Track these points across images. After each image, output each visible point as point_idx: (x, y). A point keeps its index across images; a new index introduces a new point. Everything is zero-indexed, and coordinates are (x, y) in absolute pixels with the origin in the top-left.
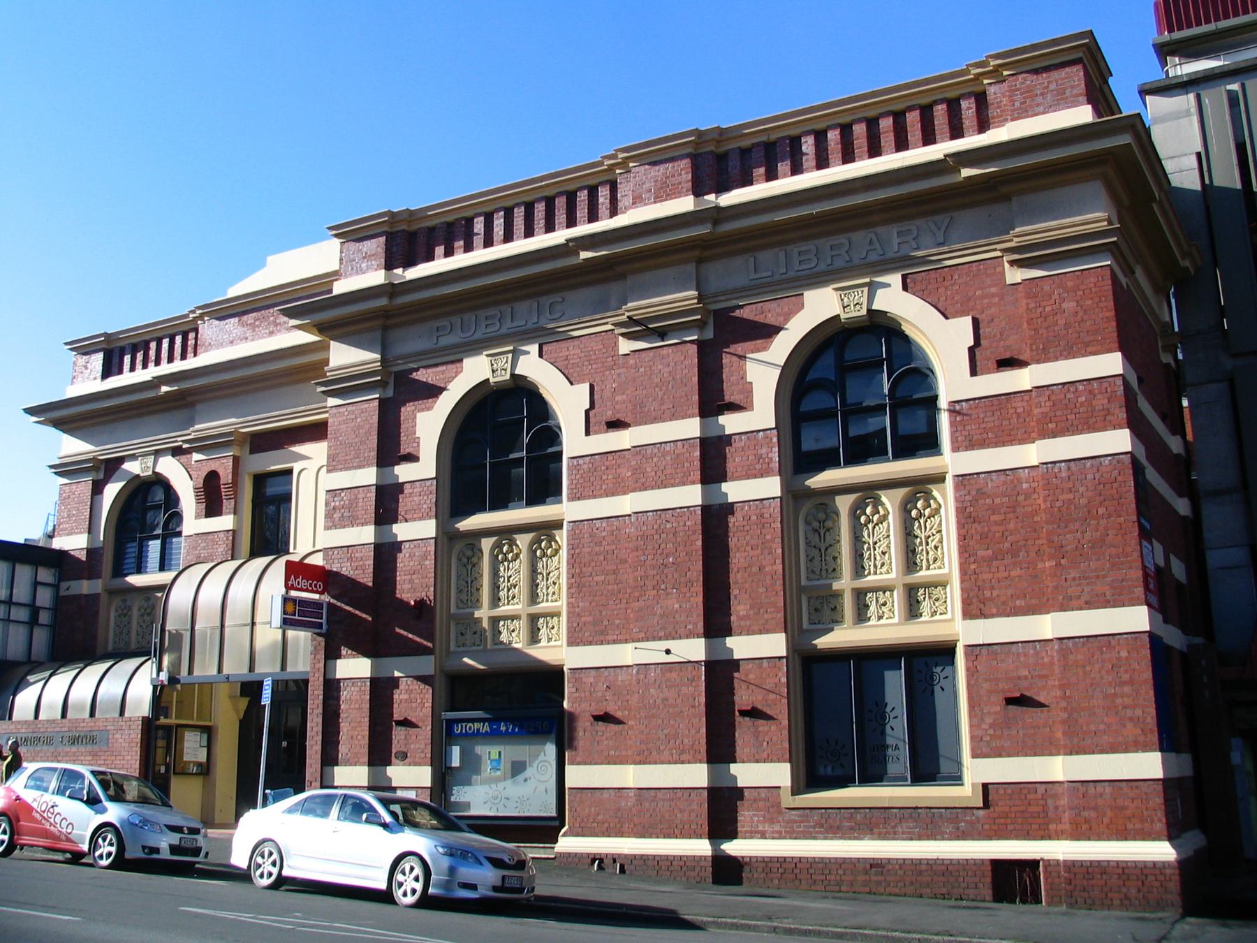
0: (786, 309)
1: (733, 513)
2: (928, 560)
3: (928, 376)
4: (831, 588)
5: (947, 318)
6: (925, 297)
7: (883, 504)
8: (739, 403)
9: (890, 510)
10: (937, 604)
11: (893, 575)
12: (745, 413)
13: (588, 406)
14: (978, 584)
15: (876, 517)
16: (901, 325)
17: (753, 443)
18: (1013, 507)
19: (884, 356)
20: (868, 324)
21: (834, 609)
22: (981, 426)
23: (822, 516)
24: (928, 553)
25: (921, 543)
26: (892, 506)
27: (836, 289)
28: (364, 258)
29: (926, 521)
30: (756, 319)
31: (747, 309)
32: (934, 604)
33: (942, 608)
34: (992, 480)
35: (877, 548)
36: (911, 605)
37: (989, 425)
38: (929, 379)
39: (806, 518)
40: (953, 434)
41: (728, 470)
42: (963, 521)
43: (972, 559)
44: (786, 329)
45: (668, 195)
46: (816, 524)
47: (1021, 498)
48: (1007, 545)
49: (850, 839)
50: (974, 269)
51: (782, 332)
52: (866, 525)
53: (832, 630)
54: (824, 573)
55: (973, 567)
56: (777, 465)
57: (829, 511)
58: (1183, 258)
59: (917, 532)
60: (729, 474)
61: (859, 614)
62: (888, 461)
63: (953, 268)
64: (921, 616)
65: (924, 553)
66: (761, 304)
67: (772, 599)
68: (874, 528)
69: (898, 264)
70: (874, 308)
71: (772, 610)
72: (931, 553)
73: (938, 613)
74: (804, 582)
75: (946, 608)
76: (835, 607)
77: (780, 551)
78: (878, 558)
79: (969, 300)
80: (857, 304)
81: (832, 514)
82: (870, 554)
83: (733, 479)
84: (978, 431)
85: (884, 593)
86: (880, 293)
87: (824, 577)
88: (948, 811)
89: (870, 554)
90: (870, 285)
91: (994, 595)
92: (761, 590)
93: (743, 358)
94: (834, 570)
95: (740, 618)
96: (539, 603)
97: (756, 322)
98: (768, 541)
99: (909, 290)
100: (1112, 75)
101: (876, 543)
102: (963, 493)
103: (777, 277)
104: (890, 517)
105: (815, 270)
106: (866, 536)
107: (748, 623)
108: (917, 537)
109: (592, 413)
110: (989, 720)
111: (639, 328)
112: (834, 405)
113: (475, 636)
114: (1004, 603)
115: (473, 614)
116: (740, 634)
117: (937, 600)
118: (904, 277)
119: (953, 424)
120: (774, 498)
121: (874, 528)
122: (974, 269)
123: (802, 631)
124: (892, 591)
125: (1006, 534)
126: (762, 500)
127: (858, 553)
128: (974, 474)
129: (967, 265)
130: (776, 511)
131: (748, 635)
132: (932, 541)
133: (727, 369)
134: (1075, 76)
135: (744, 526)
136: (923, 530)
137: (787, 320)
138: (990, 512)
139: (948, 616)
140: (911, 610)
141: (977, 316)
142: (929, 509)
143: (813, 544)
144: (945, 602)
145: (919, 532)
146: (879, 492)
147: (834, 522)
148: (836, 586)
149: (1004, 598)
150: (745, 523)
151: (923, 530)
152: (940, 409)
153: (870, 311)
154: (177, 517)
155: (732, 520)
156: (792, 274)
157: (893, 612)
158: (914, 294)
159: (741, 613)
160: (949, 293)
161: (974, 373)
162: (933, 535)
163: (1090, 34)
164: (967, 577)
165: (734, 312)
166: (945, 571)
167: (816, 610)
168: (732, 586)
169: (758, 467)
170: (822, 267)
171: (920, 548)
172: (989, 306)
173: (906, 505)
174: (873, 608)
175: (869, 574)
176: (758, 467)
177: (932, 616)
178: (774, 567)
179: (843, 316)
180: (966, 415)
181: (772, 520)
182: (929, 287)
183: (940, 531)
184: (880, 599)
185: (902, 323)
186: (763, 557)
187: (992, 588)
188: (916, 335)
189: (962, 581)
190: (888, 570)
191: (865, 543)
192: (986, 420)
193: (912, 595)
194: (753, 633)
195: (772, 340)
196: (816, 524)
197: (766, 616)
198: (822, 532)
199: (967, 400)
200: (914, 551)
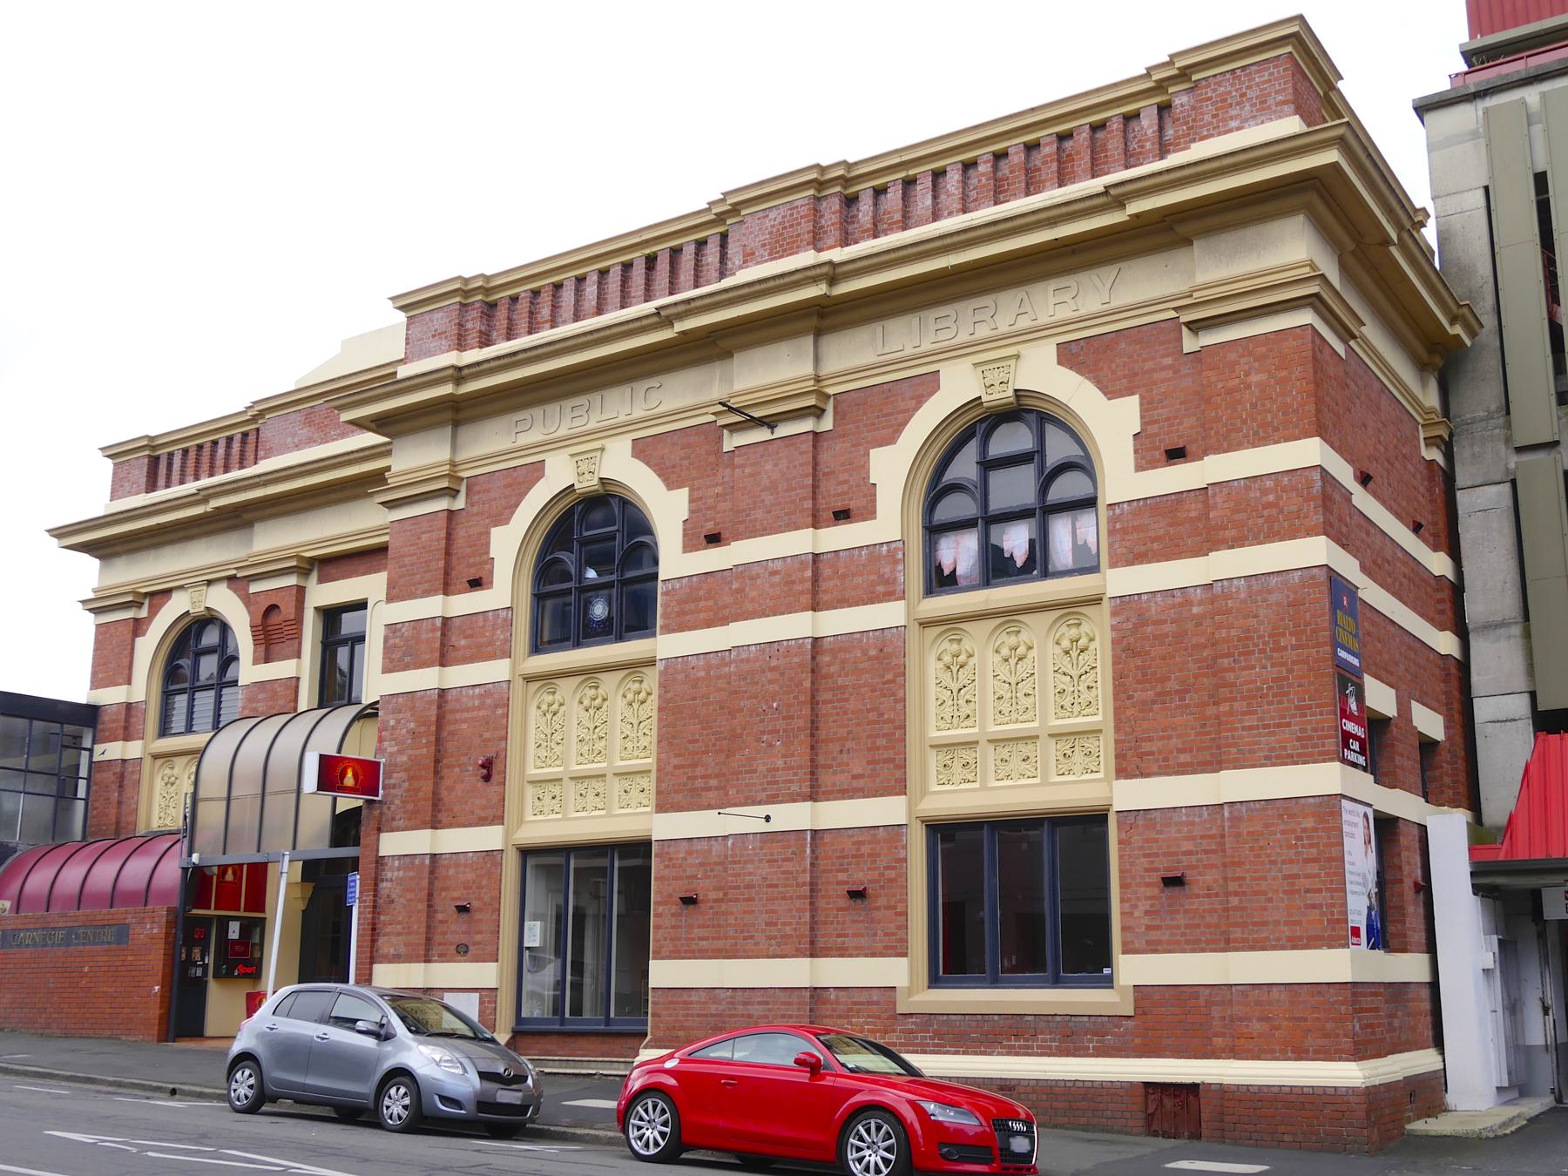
18: (1180, 636)
28: (434, 336)
45: (785, 250)
47: (1190, 626)
49: (976, 1053)
58: (1452, 322)
88: (1093, 1019)
100: (1341, 78)
110: (1144, 905)
111: (741, 419)
113: (554, 801)
134: (1278, 82)
154: (229, 661)
163: (1301, 18)
198: (955, 669)
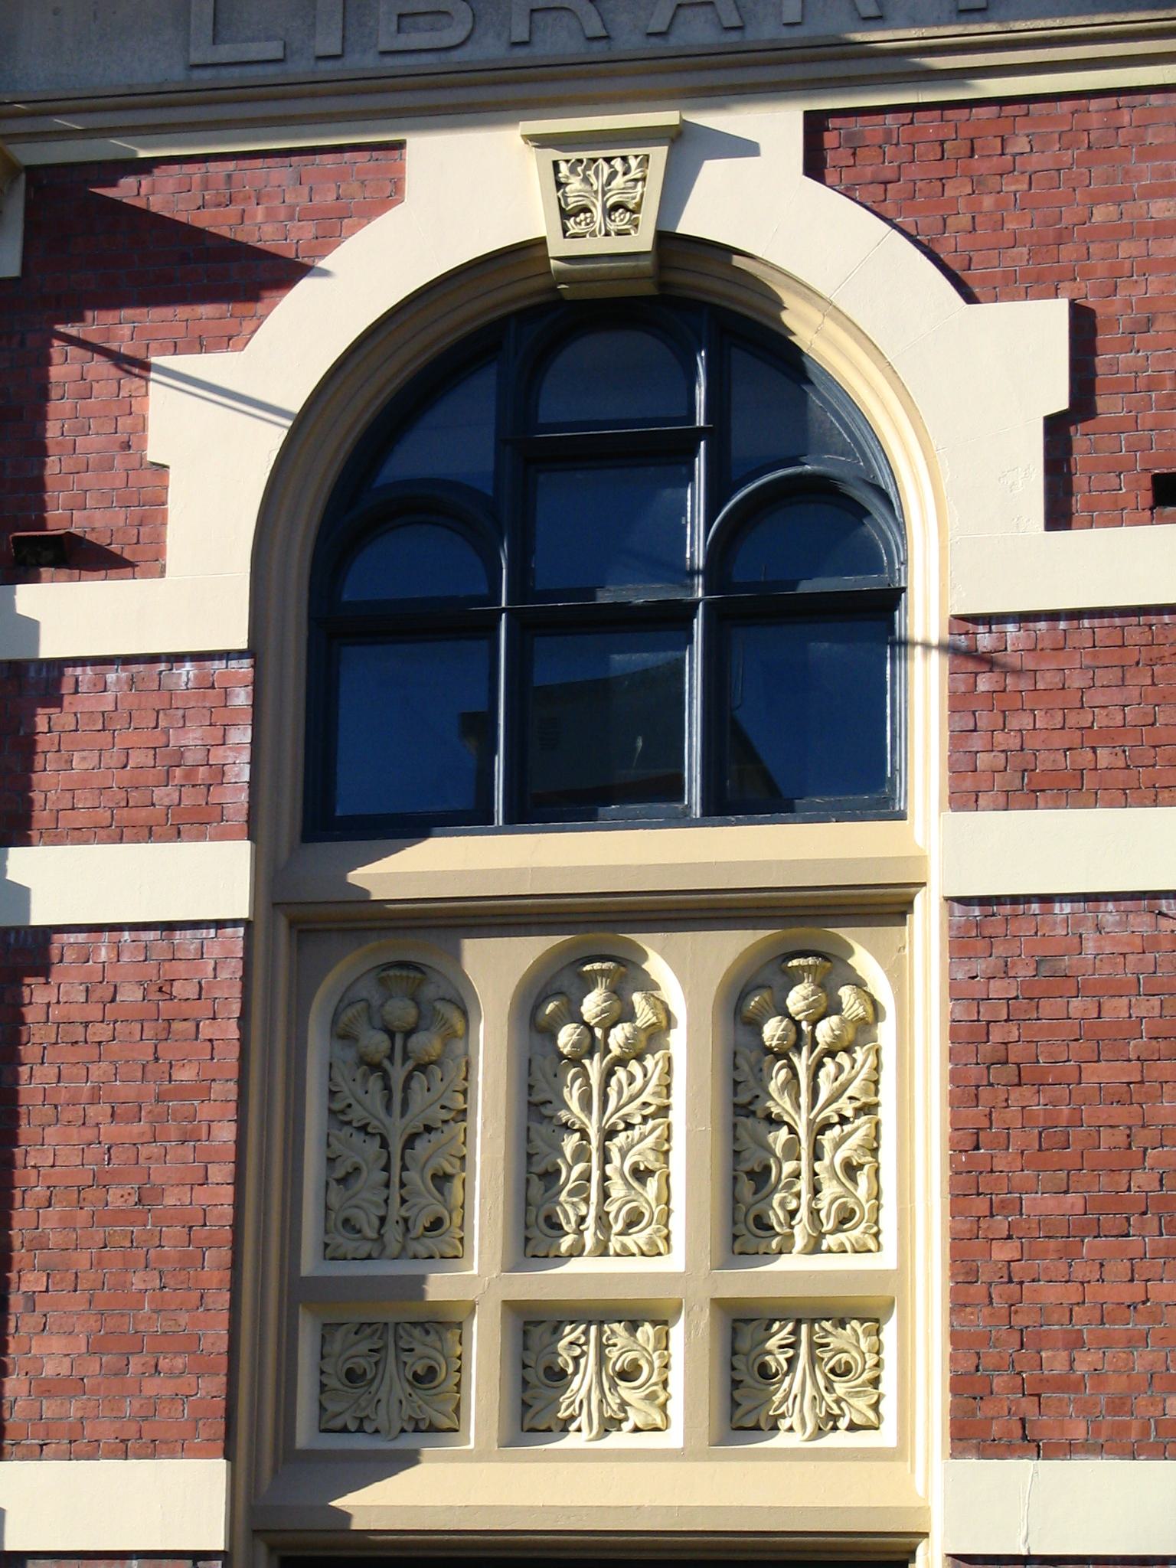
0: (327, 198)
1: (43, 970)
2: (814, 1213)
3: (867, 514)
4: (421, 1293)
5: (970, 298)
6: (889, 208)
7: (649, 986)
8: (103, 541)
9: (679, 1008)
10: (841, 1387)
11: (674, 1262)
12: (139, 583)
13: (1060, 401)
14: (1018, 1321)
15: (619, 1036)
16: (780, 305)
17: (154, 701)
19: (700, 421)
20: (648, 289)
21: (425, 1378)
22: (1073, 720)
23: (401, 1011)
24: (816, 1190)
25: (792, 1150)
26: (690, 996)
27: (542, 141)
29: (820, 1065)
30: (203, 220)
31: (167, 179)
32: (830, 1389)
33: (862, 1403)
34: (1098, 928)
35: (615, 1155)
36: (736, 1384)
37: (1101, 719)
38: (868, 527)
39: (334, 1022)
40: (958, 739)
41: (37, 796)
42: (975, 1073)
43: (1000, 1223)
44: (325, 273)
46: (375, 1042)
48: (1143, 1180)
50: (1095, 120)
51: (305, 284)
52: (576, 1061)
53: (410, 1459)
54: (392, 1233)
55: (1003, 1252)
56: (244, 797)
57: (429, 992)
59: (780, 1103)
60: (41, 816)
61: (526, 1406)
62: (682, 820)
63: (1009, 110)
64: (775, 1428)
65: (803, 1185)
66: (231, 165)
67: (184, 1318)
68: (609, 1074)
69: (798, 72)
70: (683, 228)
71: (179, 1362)
72: (830, 1189)
73: (843, 1423)
74: (310, 1264)
75: (875, 1407)
76: (432, 1371)
77: (226, 1133)
78: (617, 1189)
79: (1060, 240)
80: (616, 207)
81: (439, 1005)
82: (586, 1177)
83: (57, 837)
84: (1059, 740)
85: (633, 1326)
86: (713, 173)
87: (394, 1248)
89: (586, 1177)
90: (675, 137)
91: (1081, 1368)
92: (138, 1281)
93: (137, 366)
94: (437, 1224)
95: (48, 1389)
96: (561, 1258)
97: (202, 232)
98: (182, 1092)
99: (831, 175)
101: (610, 1134)
102: (980, 966)
103: (300, 67)
104: (678, 1041)
105: (456, 56)
106: (574, 1104)
107: (74, 1409)
108: (775, 1122)
109: (1080, 438)
112: (484, 590)
114: (1119, 1405)
115: (422, 1279)
116: (39, 1453)
117: (843, 1371)
118: (815, 125)
119: (959, 702)
120: (219, 924)
121: (609, 1074)
122: (1095, 120)
123: (288, 1455)
124: (662, 1323)
125: (1142, 1137)
126: (170, 927)
127: (539, 1168)
128: (1028, 899)
129: (1066, 106)
130: (223, 975)
131: (70, 1456)
132: (838, 1145)
133: (67, 403)
135: (86, 1024)
136: (804, 1099)
137: (330, 236)
138: (1086, 1047)
139: (886, 1437)
140: (735, 1404)
141: (1091, 302)
142: (833, 1020)
143: (357, 1115)
144: (875, 1382)
145: (786, 1103)
146: (640, 939)
147: (450, 1036)
148: (440, 1287)
149: (1116, 1385)
150: (94, 1012)
151: (804, 1099)
152: (905, 643)
153: (666, 239)
155: (38, 995)
156: (363, 61)
157: (663, 1407)
158: (848, 193)
159: (49, 1370)
160: (988, 202)
161: (1058, 516)
162: (843, 1120)
164: (979, 1289)
165: (113, 184)
166: (885, 1260)
167: (352, 1376)
168: (19, 1255)
169: (164, 796)
170: (490, 49)
171: (788, 1167)
172: (1148, 266)
173: (743, 996)
174: (582, 1384)
175: (577, 1251)
176: (164, 796)
177: (819, 1432)
178: (202, 1195)
179: (559, 247)
180: (1018, 672)
181: (203, 1009)
182: (913, 171)
183: (868, 1109)
184: (613, 1353)
185: (787, 298)
186: (154, 1149)
187: (1075, 1342)
188: (841, 351)
189: (958, 1305)
190: (651, 1242)
191: (567, 1128)
192: (1094, 697)
193: (744, 1344)
194: (93, 1452)
195: (259, 307)
196: (375, 1042)
197: (151, 1387)
198: (398, 1073)
199: (1024, 618)
200: (761, 1177)
